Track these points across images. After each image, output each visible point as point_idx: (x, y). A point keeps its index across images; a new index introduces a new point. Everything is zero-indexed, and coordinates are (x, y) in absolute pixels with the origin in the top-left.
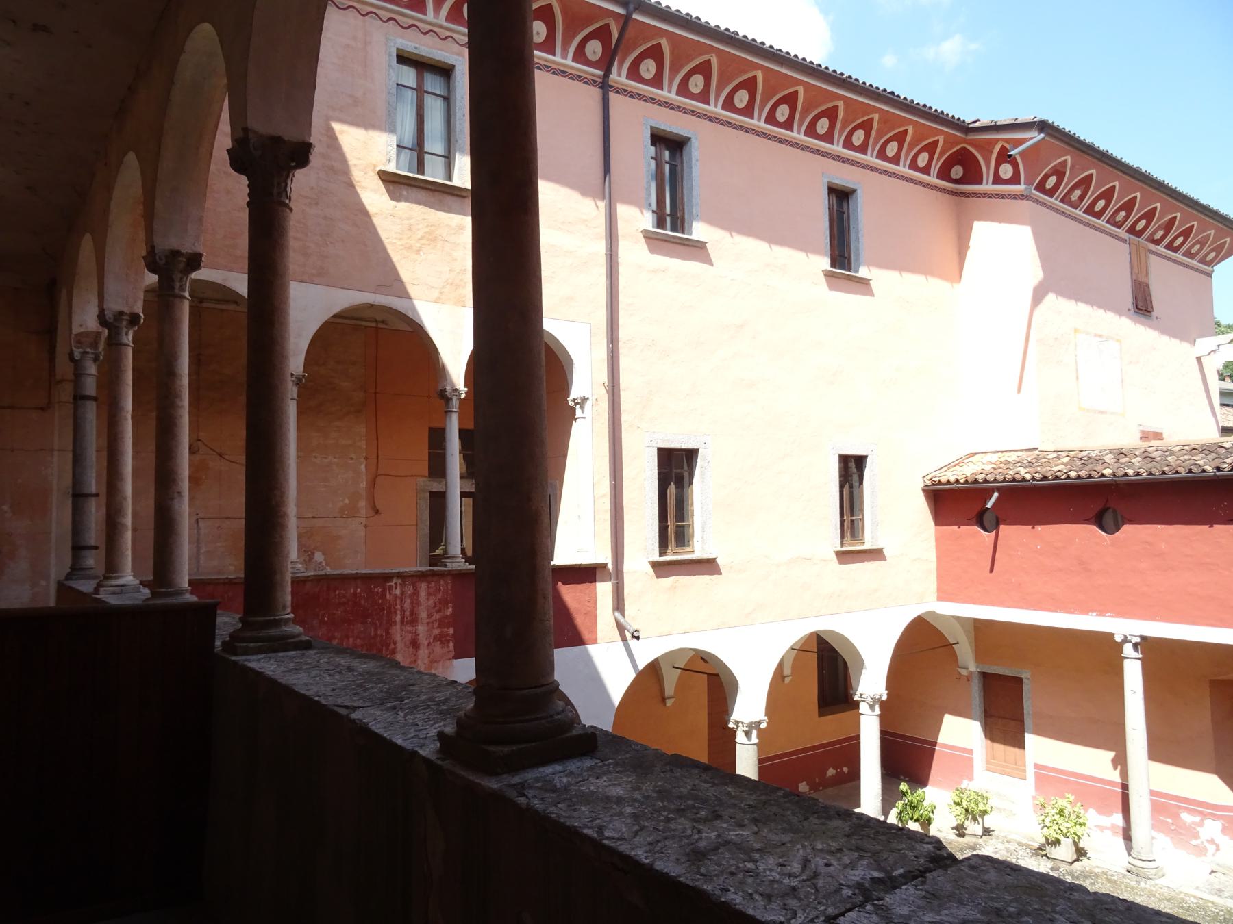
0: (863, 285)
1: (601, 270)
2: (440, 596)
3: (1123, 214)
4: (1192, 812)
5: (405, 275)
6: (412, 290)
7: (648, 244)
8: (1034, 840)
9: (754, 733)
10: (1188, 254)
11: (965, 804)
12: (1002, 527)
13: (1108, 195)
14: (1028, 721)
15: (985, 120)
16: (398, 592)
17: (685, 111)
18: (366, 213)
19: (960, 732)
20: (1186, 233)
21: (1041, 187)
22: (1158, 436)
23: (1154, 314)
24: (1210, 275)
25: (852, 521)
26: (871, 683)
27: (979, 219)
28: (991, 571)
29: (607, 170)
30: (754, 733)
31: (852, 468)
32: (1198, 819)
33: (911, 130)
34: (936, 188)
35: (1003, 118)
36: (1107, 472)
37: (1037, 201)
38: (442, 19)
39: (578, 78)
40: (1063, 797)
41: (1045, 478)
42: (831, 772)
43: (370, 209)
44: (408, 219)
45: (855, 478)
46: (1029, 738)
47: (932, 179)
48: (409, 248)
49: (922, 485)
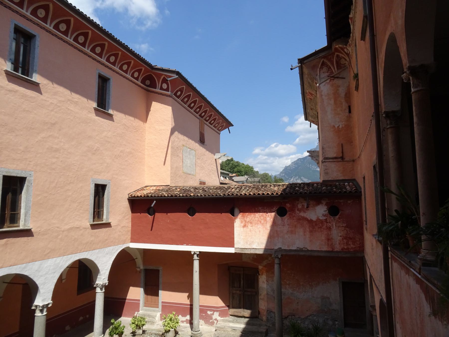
0: (110, 117)
3: (198, 109)
4: (211, 310)
7: (7, 77)
8: (160, 331)
9: (45, 310)
10: (214, 126)
11: (136, 323)
12: (156, 214)
13: (195, 102)
14: (161, 286)
15: (159, 66)
19: (136, 293)
20: (214, 120)
21: (175, 94)
22: (204, 183)
23: (205, 143)
24: (219, 134)
25: (99, 212)
26: (102, 279)
27: (154, 101)
28: (151, 230)
30: (45, 310)
31: (100, 190)
32: (212, 313)
33: (133, 62)
34: (140, 86)
35: (165, 67)
36: (192, 194)
37: (174, 99)
40: (172, 313)
41: (172, 196)
42: (81, 318)
45: (101, 193)
46: (160, 292)
47: (139, 83)
49: (127, 197)
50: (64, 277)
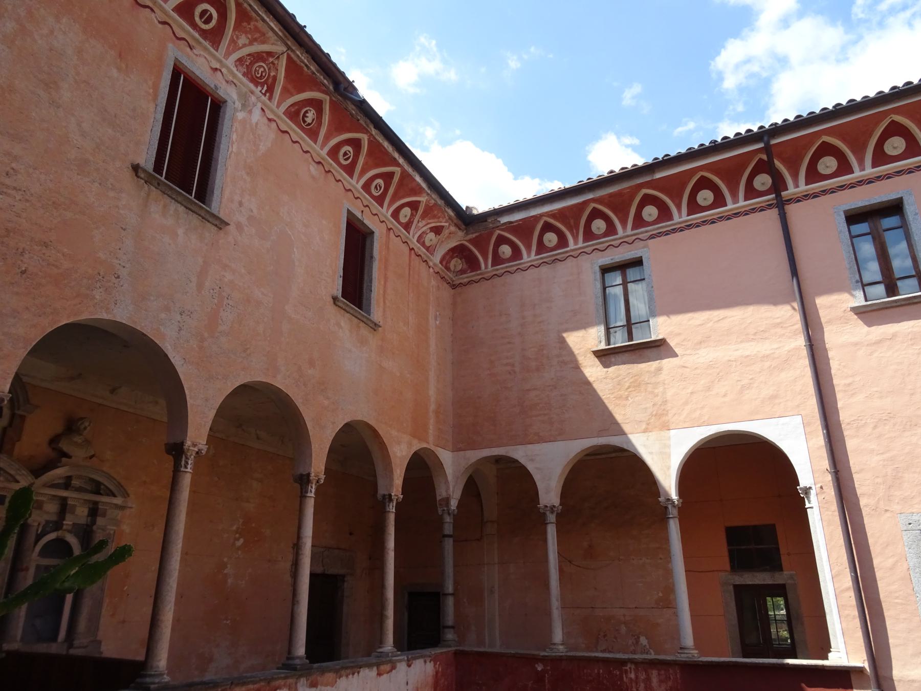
1: (804, 363)
2: (670, 683)
5: (619, 418)
6: (626, 428)
16: (633, 676)
17: (888, 176)
18: (588, 383)
29: (794, 272)
38: (415, 240)
39: (753, 210)
43: (591, 379)
44: (617, 377)
48: (620, 397)
50: (626, 454)
